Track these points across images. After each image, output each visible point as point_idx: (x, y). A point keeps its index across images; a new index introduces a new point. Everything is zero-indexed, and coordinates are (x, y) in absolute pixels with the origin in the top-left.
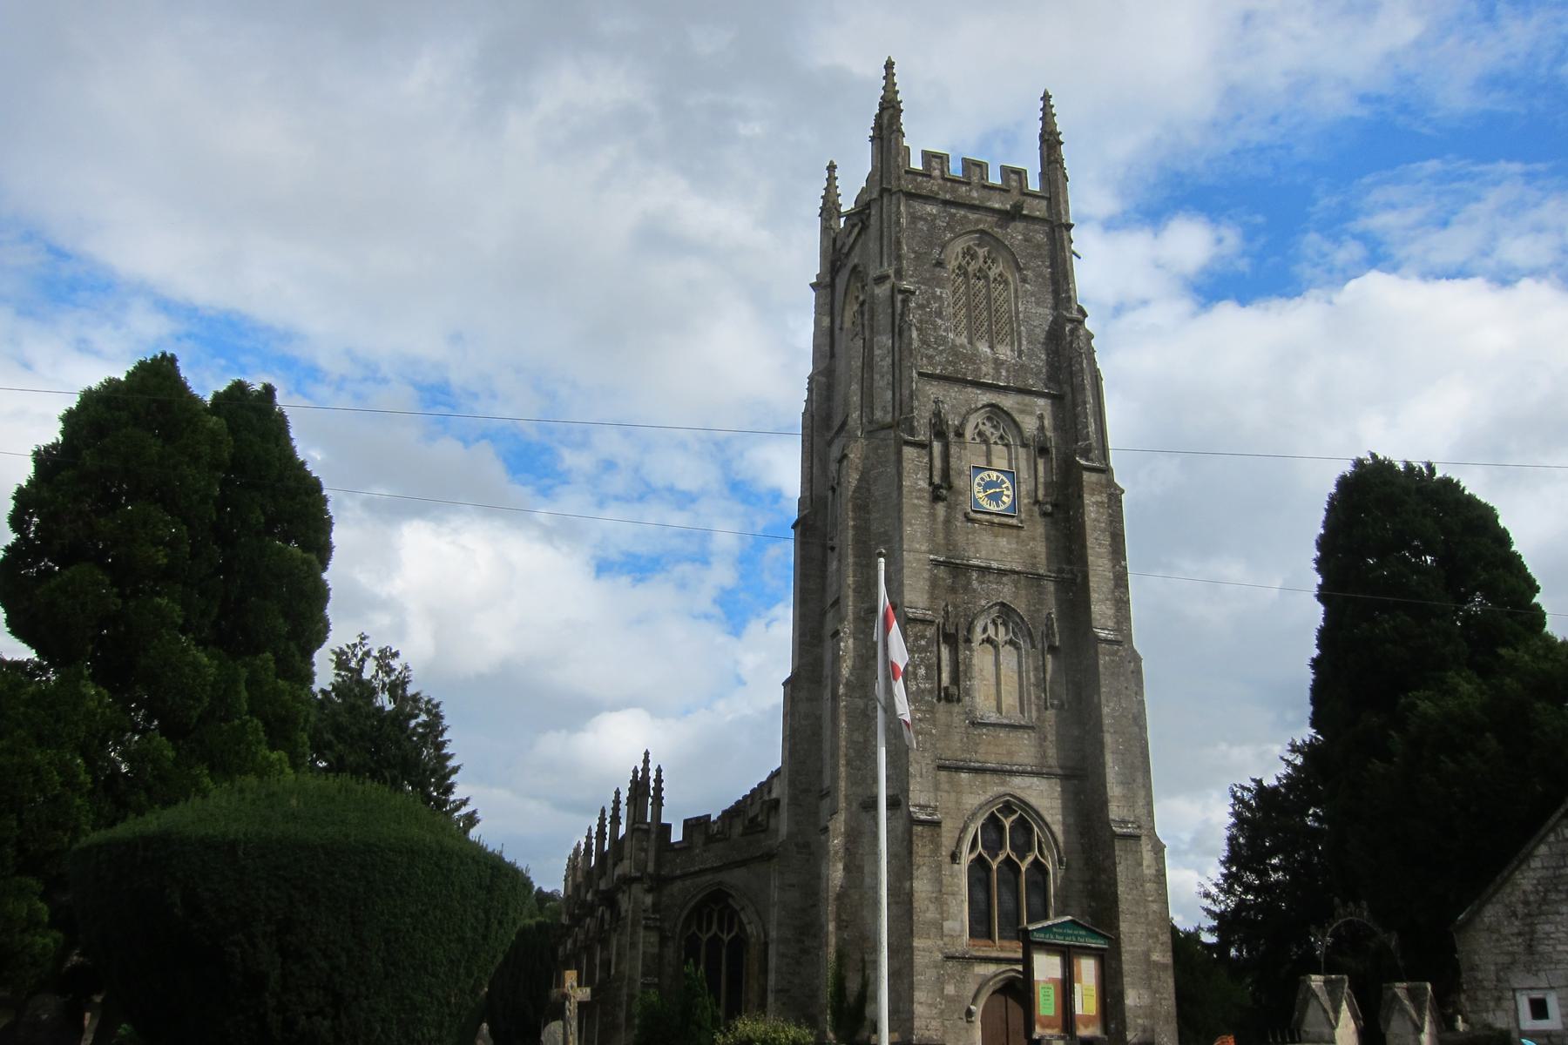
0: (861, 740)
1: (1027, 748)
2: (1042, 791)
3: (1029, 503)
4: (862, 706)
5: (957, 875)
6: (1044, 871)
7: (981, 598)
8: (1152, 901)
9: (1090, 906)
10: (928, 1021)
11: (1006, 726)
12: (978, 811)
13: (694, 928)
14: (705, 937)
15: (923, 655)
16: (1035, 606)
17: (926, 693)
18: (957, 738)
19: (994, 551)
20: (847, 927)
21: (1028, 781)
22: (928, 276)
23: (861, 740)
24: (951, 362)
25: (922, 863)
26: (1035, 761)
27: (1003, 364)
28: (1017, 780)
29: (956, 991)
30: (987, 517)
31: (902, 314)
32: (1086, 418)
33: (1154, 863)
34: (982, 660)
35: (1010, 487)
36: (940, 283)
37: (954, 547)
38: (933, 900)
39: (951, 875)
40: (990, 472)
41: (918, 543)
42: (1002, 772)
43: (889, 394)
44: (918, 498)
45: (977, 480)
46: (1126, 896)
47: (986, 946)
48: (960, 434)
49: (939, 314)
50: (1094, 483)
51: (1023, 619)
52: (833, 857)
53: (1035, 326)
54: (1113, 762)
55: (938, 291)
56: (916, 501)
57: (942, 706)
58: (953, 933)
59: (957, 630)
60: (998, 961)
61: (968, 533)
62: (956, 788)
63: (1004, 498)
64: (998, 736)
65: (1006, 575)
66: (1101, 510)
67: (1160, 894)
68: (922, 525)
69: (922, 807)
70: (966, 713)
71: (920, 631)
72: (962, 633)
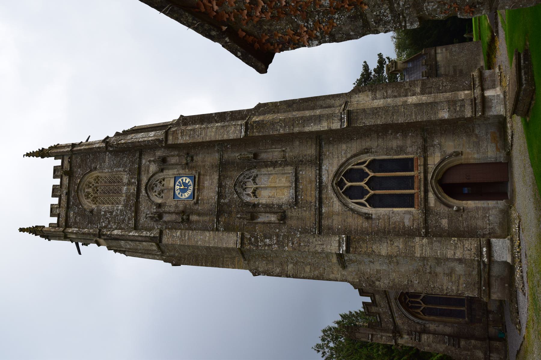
0: (309, 267)
1: (307, 172)
2: (329, 163)
3: (188, 169)
4: (292, 265)
5: (378, 216)
6: (373, 161)
7: (233, 198)
8: (387, 93)
9: (392, 134)
10: (466, 249)
11: (296, 184)
12: (342, 202)
13: (419, 311)
14: (423, 306)
15: (259, 240)
16: (235, 167)
17: (279, 239)
18: (304, 214)
19: (211, 189)
20: (411, 281)
21: (324, 172)
22: (97, 218)
23: (309, 267)
24: (130, 208)
25: (371, 249)
26: (314, 167)
27: (129, 181)
28: (324, 178)
29: (446, 218)
30: (196, 191)
31: (107, 236)
32: (145, 141)
33: (365, 92)
34: (264, 197)
35: (182, 178)
36: (99, 211)
37: (210, 211)
38: (392, 242)
39: (379, 220)
40: (176, 189)
41: (205, 238)
42: (320, 188)
43: (144, 243)
44: (185, 237)
45: (179, 196)
46: (383, 119)
47: (418, 198)
48: (159, 206)
49: (111, 213)
50: (173, 138)
51: (241, 174)
52: (372, 287)
53: (113, 163)
54: (309, 126)
55: (103, 213)
56: (186, 238)
57: (289, 222)
58: (411, 219)
59: (249, 212)
60: (426, 192)
61: (204, 203)
62: (331, 215)
63: (187, 182)
64: (302, 189)
65: (221, 183)
66: (185, 133)
67: (382, 88)
68: (197, 234)
69: (340, 246)
70: (291, 208)
71: (247, 241)
72: (250, 209)
